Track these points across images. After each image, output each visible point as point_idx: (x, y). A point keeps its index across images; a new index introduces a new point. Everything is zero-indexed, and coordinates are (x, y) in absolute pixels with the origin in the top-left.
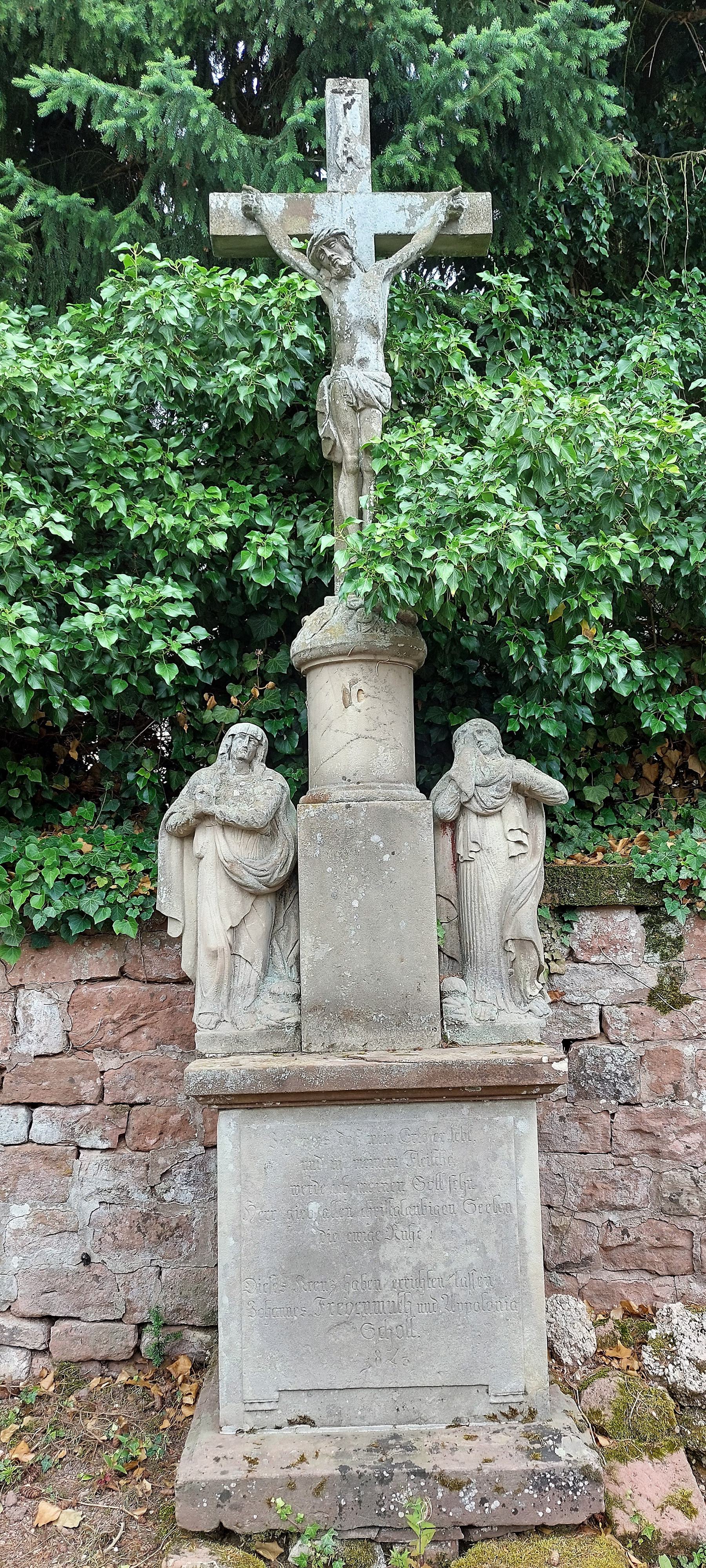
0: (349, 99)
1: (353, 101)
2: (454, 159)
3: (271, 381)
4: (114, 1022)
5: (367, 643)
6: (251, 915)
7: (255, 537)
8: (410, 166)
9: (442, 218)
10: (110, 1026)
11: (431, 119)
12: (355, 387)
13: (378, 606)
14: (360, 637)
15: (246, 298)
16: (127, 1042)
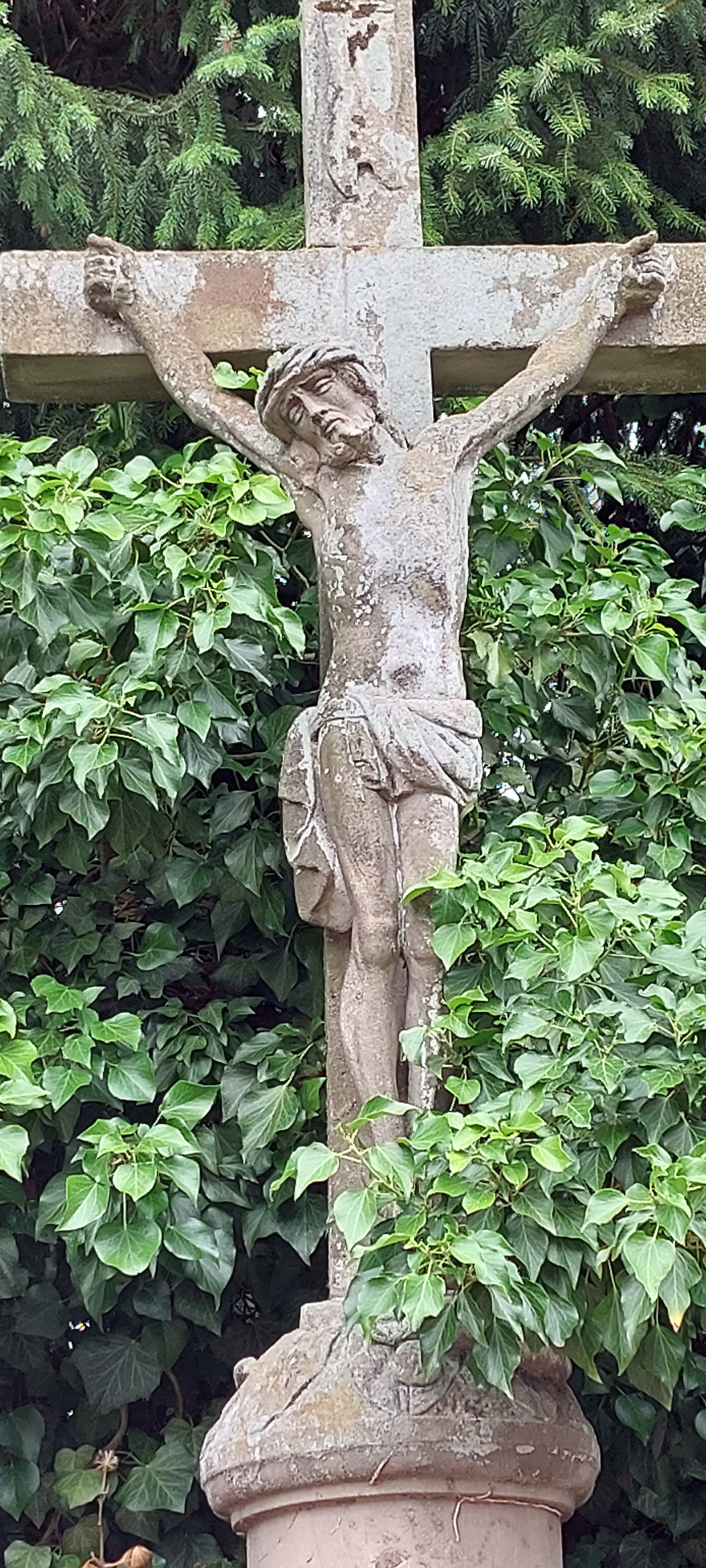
0: (362, 25)
1: (372, 29)
2: (628, 143)
3: (159, 731)
5: (426, 1446)
7: (106, 1137)
8: (514, 170)
9: (609, 309)
11: (568, 57)
12: (384, 742)
13: (461, 1343)
14: (404, 1427)
15: (96, 522)
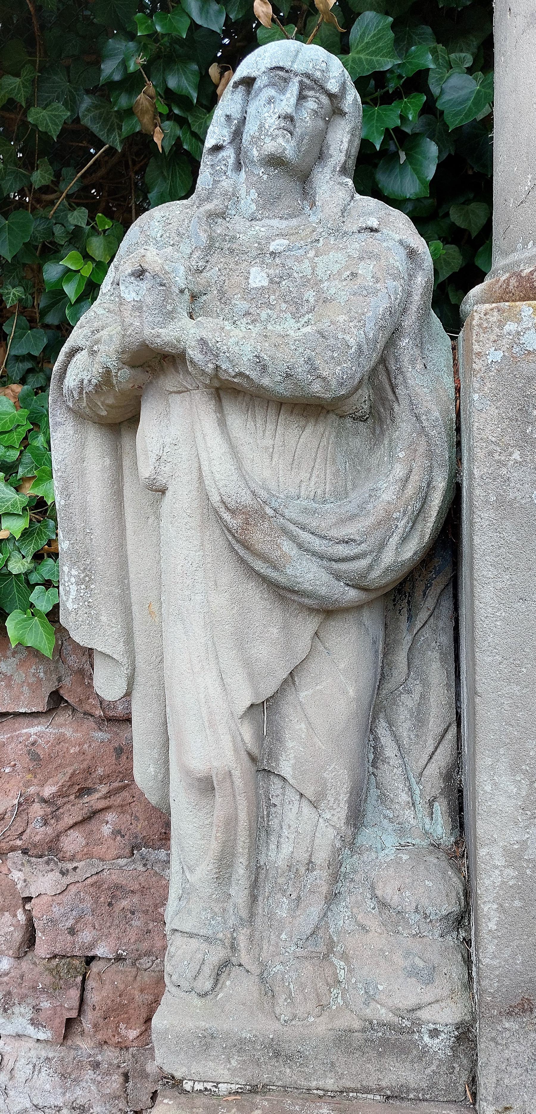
4: (44, 801)
6: (313, 666)
10: (37, 810)
16: (73, 842)
